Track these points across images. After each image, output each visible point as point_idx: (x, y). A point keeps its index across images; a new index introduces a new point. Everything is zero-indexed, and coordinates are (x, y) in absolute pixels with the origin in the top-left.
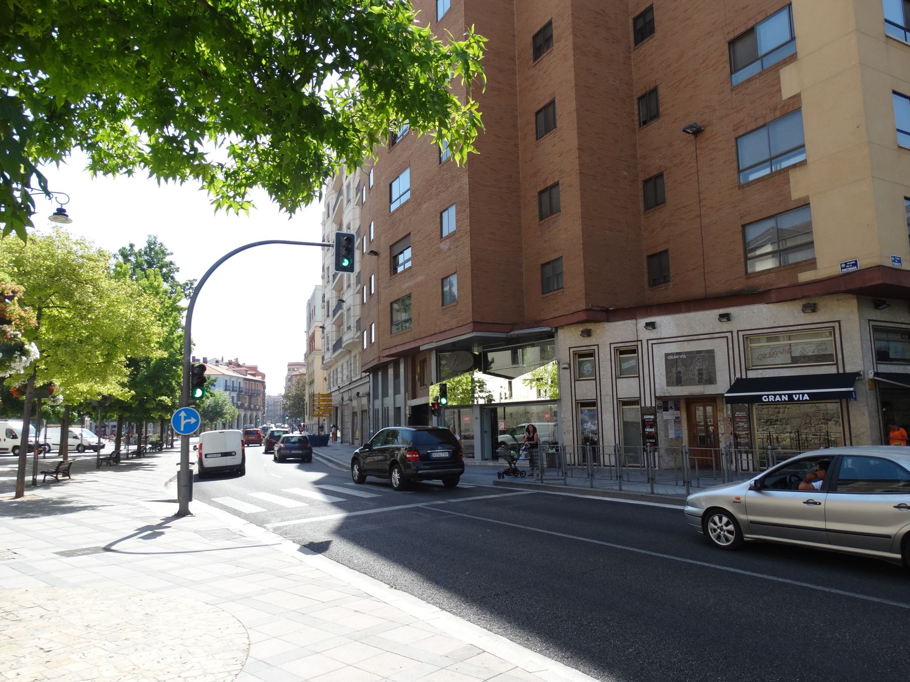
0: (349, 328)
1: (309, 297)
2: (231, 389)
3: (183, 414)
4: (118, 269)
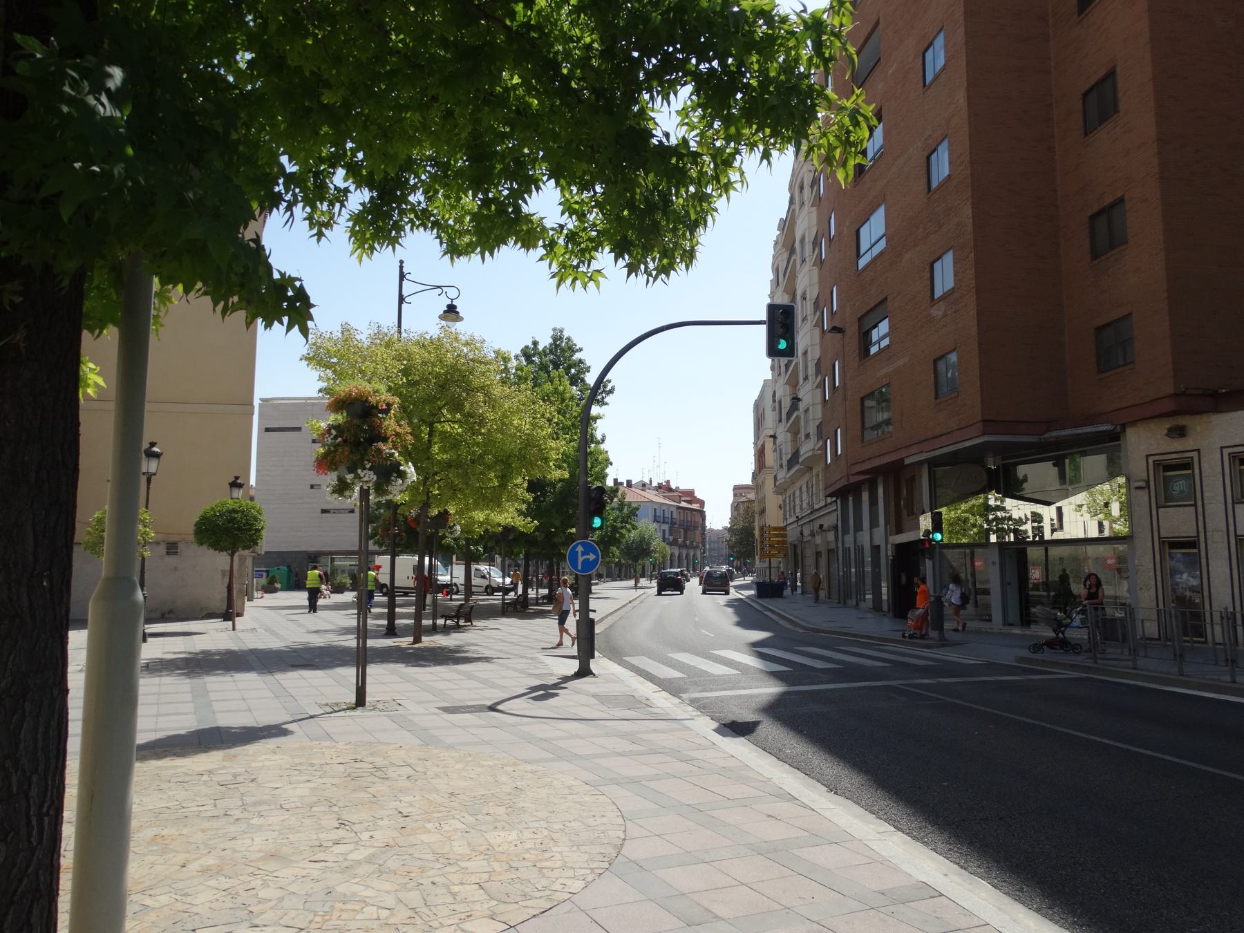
0: (808, 436)
1: (755, 395)
2: (662, 521)
3: (580, 549)
4: (519, 372)
